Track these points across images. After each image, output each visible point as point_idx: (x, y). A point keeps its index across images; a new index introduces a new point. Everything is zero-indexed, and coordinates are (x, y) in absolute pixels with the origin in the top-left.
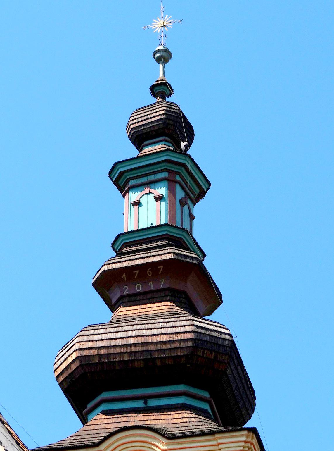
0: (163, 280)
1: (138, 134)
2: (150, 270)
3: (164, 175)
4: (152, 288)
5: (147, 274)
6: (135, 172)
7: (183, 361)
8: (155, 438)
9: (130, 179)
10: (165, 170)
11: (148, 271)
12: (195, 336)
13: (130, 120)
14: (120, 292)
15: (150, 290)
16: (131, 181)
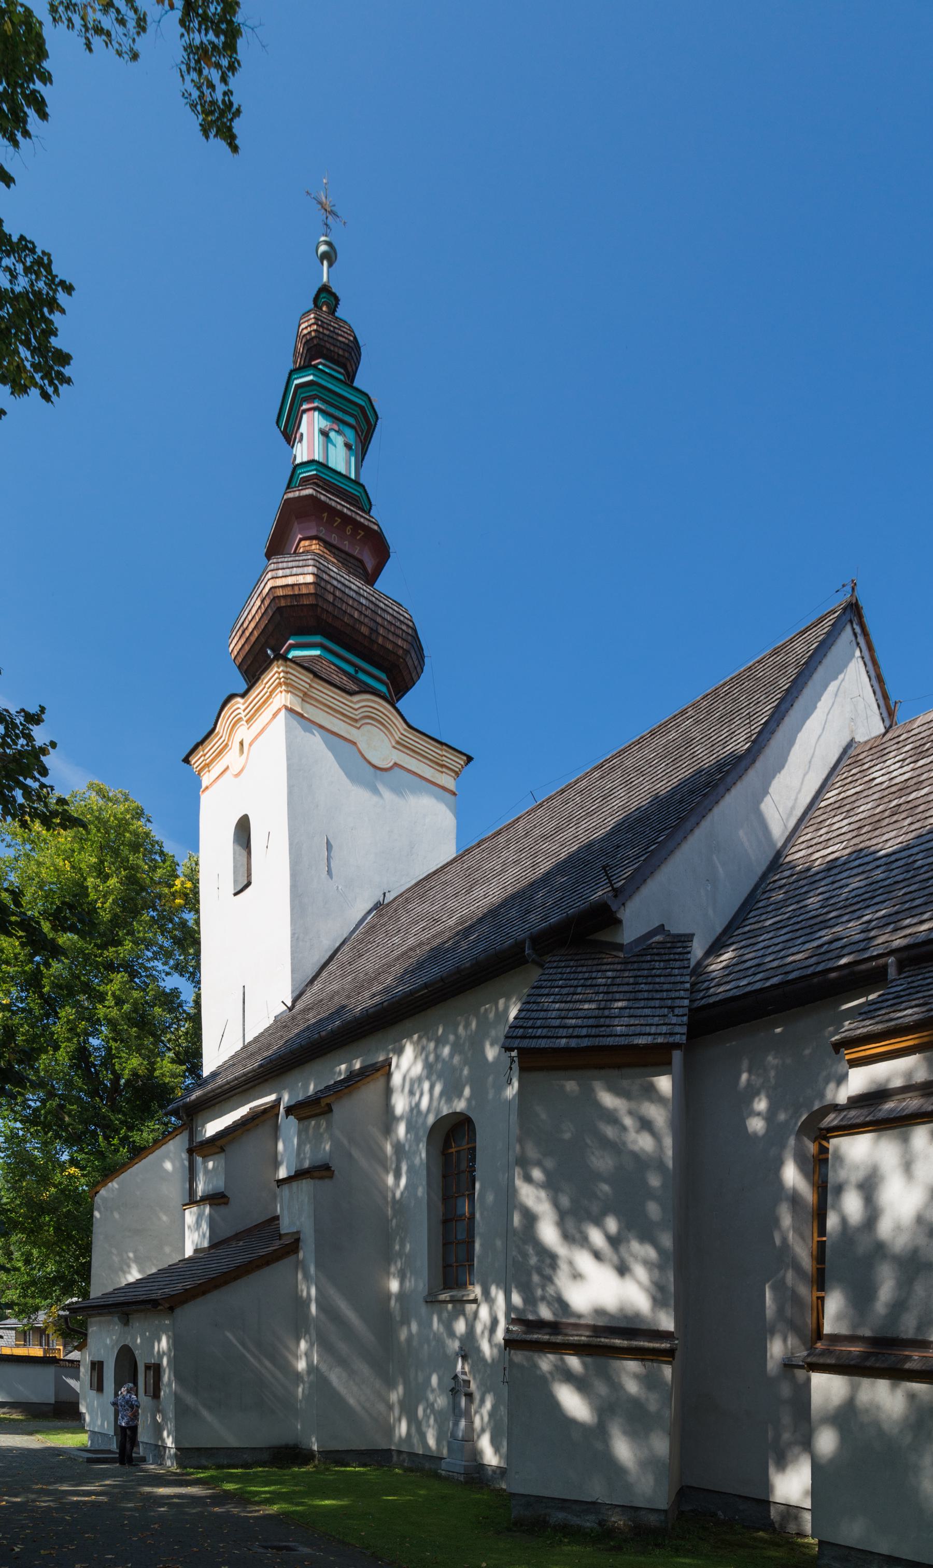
3: (351, 421)
11: (348, 528)
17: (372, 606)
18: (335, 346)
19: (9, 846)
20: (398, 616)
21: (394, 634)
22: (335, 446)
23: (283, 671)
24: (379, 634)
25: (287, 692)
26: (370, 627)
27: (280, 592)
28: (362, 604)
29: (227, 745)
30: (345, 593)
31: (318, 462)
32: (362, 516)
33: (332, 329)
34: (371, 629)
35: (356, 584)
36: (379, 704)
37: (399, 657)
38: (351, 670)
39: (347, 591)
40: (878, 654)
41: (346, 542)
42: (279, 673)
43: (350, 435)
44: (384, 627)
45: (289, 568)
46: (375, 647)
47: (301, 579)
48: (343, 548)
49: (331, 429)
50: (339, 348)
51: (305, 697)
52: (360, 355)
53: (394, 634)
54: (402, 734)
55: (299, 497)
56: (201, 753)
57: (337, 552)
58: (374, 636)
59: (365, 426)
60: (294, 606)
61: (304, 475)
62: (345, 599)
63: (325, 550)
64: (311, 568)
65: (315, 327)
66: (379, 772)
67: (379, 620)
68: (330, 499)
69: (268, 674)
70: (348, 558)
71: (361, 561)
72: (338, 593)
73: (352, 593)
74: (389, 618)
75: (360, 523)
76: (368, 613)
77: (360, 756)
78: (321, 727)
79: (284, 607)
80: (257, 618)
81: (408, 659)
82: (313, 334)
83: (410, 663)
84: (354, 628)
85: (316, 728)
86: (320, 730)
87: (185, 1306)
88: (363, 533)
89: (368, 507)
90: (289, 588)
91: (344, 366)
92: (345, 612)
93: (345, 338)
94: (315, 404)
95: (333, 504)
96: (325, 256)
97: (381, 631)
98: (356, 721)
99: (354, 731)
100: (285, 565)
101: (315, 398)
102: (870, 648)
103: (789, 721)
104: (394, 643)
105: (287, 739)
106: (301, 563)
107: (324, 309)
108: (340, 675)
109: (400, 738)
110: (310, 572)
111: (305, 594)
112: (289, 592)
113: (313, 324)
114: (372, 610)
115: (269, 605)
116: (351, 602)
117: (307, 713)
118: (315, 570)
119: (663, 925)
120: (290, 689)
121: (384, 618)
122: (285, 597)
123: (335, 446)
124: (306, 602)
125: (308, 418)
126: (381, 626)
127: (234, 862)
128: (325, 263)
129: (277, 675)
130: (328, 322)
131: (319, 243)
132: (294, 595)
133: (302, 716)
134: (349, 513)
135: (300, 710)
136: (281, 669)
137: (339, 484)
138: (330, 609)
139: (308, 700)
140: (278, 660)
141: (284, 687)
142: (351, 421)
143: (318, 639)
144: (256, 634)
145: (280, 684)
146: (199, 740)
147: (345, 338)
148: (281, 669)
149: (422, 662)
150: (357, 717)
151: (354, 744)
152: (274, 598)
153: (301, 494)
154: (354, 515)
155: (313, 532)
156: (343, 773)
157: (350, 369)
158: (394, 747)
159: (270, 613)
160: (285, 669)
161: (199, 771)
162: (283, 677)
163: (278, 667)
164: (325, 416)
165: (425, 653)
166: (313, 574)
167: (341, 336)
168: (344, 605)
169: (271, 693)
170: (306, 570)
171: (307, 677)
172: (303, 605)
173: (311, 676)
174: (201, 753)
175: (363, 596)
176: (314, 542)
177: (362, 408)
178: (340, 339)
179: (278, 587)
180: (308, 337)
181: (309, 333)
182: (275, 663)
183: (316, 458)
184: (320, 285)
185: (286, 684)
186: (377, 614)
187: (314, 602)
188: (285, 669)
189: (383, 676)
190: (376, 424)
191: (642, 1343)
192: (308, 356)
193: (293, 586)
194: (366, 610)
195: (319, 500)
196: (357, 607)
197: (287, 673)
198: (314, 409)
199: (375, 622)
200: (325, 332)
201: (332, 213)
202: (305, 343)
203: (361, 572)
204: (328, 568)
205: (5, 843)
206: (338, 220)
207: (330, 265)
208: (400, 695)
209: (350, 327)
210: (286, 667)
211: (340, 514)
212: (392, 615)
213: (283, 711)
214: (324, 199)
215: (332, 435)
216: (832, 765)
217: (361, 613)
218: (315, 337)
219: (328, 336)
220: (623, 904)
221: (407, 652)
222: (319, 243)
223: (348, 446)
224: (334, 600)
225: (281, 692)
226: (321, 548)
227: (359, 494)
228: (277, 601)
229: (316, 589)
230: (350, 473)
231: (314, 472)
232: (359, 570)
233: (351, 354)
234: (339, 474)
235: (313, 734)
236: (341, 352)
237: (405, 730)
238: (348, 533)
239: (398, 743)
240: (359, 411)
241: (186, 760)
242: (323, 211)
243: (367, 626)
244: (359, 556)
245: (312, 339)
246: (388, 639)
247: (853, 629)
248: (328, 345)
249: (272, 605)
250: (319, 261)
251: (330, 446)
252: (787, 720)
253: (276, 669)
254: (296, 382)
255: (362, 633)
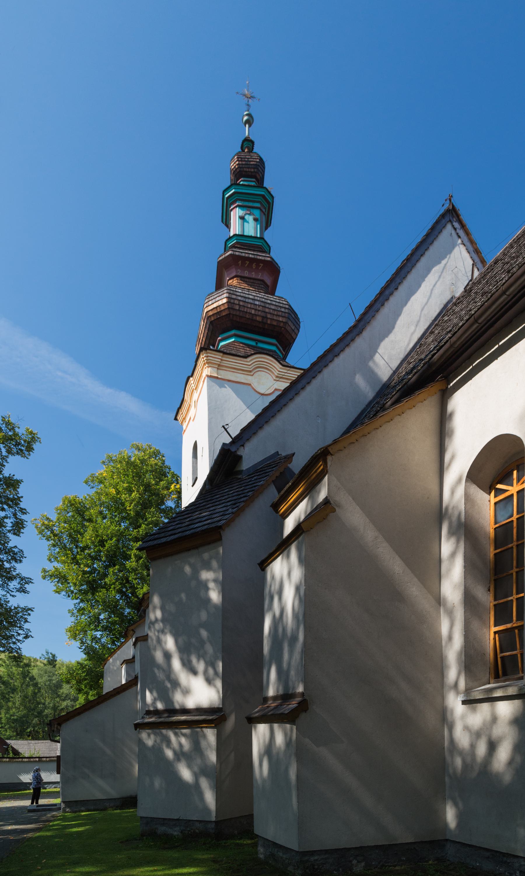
3: (258, 205)
11: (254, 265)
19: (93, 487)
21: (277, 315)
23: (205, 356)
24: (268, 318)
25: (208, 367)
27: (211, 313)
28: (256, 305)
29: (190, 405)
31: (238, 235)
32: (260, 256)
33: (247, 160)
34: (263, 317)
35: (261, 295)
37: (281, 327)
39: (247, 300)
40: (475, 236)
41: (253, 273)
42: (204, 358)
43: (257, 213)
44: (270, 313)
46: (266, 327)
47: (220, 303)
48: (251, 276)
49: (245, 214)
50: (252, 168)
51: (219, 367)
52: (264, 168)
53: (277, 315)
54: (279, 371)
55: (225, 258)
56: (181, 413)
57: (247, 280)
58: (265, 321)
61: (231, 244)
62: (246, 305)
63: (241, 282)
64: (225, 294)
65: (237, 163)
66: (265, 397)
67: (267, 310)
68: (242, 252)
70: (255, 281)
71: (262, 281)
72: (241, 303)
74: (273, 307)
76: (261, 308)
78: (229, 381)
82: (237, 167)
83: (289, 329)
86: (230, 383)
87: (68, 722)
89: (268, 249)
90: (215, 309)
91: (254, 177)
92: (246, 312)
93: (254, 161)
94: (237, 204)
95: (243, 255)
96: (247, 122)
97: (269, 316)
98: (250, 371)
99: (250, 378)
100: (212, 298)
102: (467, 233)
103: (393, 300)
105: (208, 393)
106: (220, 294)
107: (246, 151)
109: (278, 374)
110: (225, 297)
113: (236, 161)
114: (262, 306)
115: (206, 322)
116: (249, 306)
117: (221, 375)
119: (278, 452)
120: (210, 365)
121: (270, 309)
122: (213, 315)
124: (224, 314)
125: (233, 213)
126: (269, 313)
128: (247, 126)
129: (203, 359)
130: (245, 157)
131: (244, 115)
132: (218, 312)
133: (217, 378)
134: (253, 256)
135: (216, 375)
136: (204, 355)
137: (232, 243)
138: (238, 313)
140: (202, 351)
141: (207, 365)
142: (258, 205)
143: (233, 332)
144: (204, 340)
145: (205, 364)
146: (178, 406)
147: (254, 161)
148: (204, 355)
149: (297, 326)
150: (251, 369)
151: (250, 385)
154: (256, 257)
155: (234, 274)
157: (259, 177)
158: (275, 380)
159: (208, 326)
162: (206, 360)
164: (242, 208)
165: (301, 320)
166: (226, 297)
167: (252, 161)
168: (246, 308)
169: (202, 370)
171: (220, 356)
172: (223, 316)
173: (221, 354)
174: (181, 413)
175: (257, 300)
176: (235, 279)
177: (263, 196)
179: (209, 311)
180: (234, 169)
181: (235, 167)
182: (201, 353)
183: (237, 233)
184: (243, 139)
186: (265, 307)
187: (228, 313)
189: (274, 341)
190: (273, 201)
191: (179, 718)
192: (236, 179)
193: (216, 307)
194: (259, 307)
195: (236, 255)
196: (254, 307)
197: (207, 357)
198: (236, 207)
199: (265, 312)
201: (252, 97)
202: (233, 173)
203: (263, 286)
204: (236, 291)
205: (90, 487)
206: (255, 100)
207: (250, 126)
208: (287, 348)
209: (258, 154)
210: (207, 353)
211: (248, 259)
212: (275, 305)
214: (246, 92)
215: (247, 217)
216: (433, 319)
217: (256, 310)
218: (238, 168)
219: (245, 164)
220: (243, 446)
221: (286, 323)
222: (244, 115)
223: (256, 220)
224: (239, 307)
225: (206, 368)
226: (238, 281)
227: (261, 244)
229: (228, 305)
230: (257, 234)
231: (235, 241)
232: (261, 286)
233: (258, 169)
234: (251, 237)
235: (225, 387)
236: (252, 170)
237: (281, 368)
238: (254, 268)
239: (277, 377)
240: (262, 198)
241: (176, 419)
242: (246, 98)
244: (262, 278)
245: (236, 170)
246: (274, 319)
247: (453, 226)
248: (245, 169)
249: (208, 322)
250: (244, 125)
251: (245, 224)
252: (392, 299)
254: (227, 196)
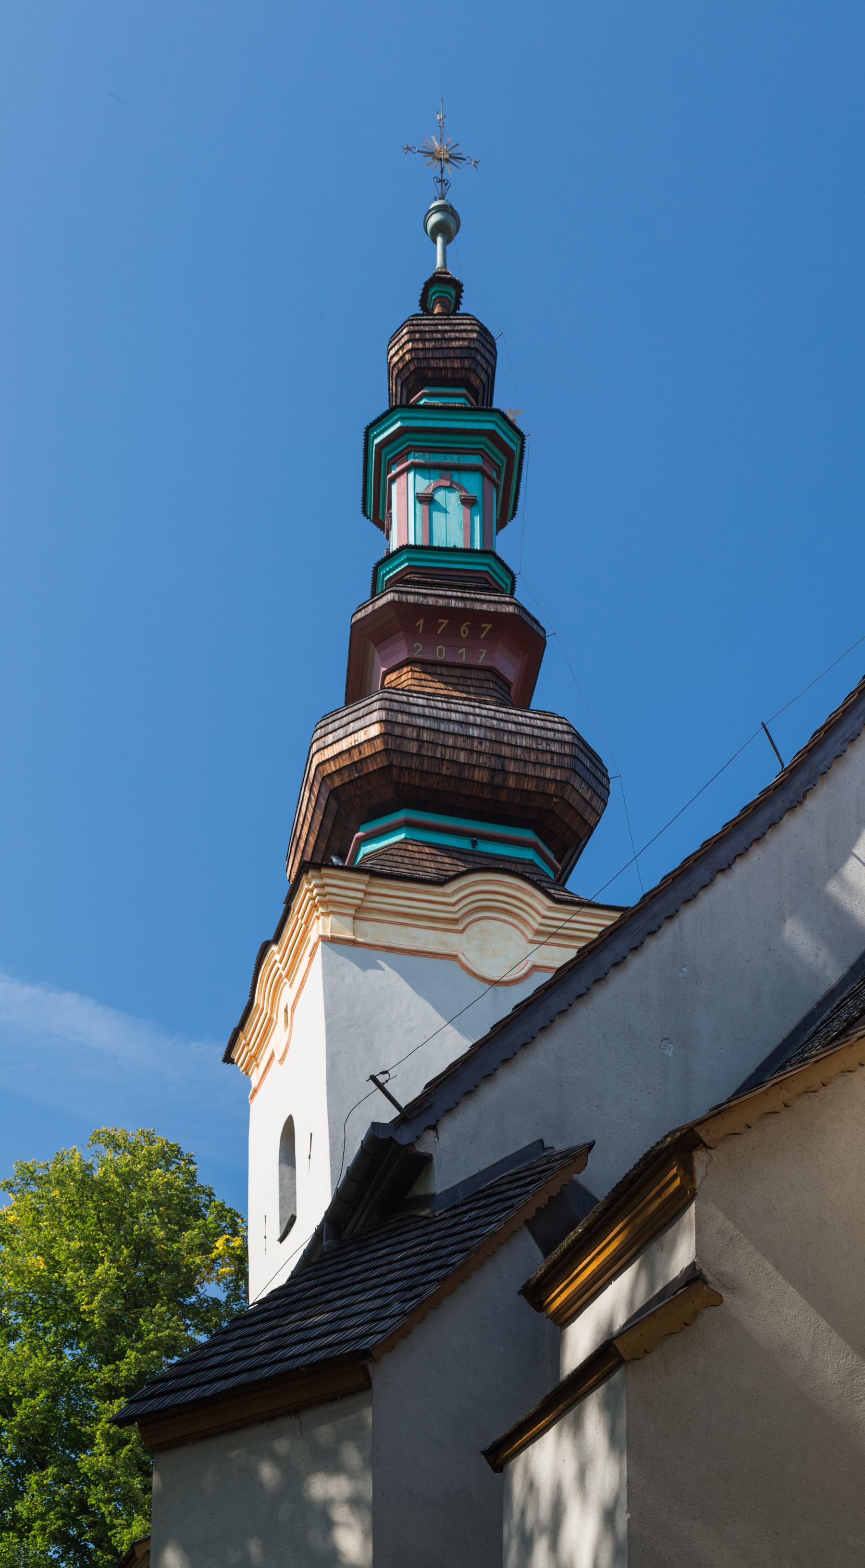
0: (485, 651)
1: (419, 365)
2: (467, 626)
3: (475, 460)
4: (464, 660)
5: (460, 633)
6: (392, 445)
7: (551, 791)
8: (532, 895)
9: (413, 449)
10: (480, 452)
11: (463, 627)
12: (466, 759)
13: (406, 324)
14: (408, 651)
15: (458, 661)
16: (413, 453)
17: (492, 735)
18: (444, 359)
20: (544, 733)
22: (446, 512)
26: (489, 768)
27: (332, 767)
28: (472, 737)
29: (271, 1019)
30: (439, 731)
36: (498, 883)
38: (464, 844)
39: (443, 727)
42: (312, 891)
43: (473, 483)
44: (516, 759)
45: (342, 727)
46: (504, 796)
47: (361, 737)
51: (359, 912)
54: (544, 917)
55: (373, 612)
56: (244, 1042)
57: (444, 671)
58: (498, 780)
59: (501, 459)
60: (356, 779)
62: (440, 739)
65: (410, 345)
67: (506, 751)
68: (425, 595)
69: (299, 897)
70: (467, 673)
72: (425, 736)
73: (452, 728)
75: (482, 612)
76: (485, 747)
77: (464, 973)
78: (390, 949)
79: (340, 786)
80: (309, 816)
81: (568, 794)
82: (407, 357)
83: (573, 799)
84: (460, 779)
85: (382, 953)
88: (489, 626)
89: (508, 581)
91: (465, 383)
93: (463, 339)
95: (431, 601)
96: (439, 228)
97: (511, 767)
98: (456, 921)
99: (454, 938)
101: (409, 453)
104: (537, 777)
108: (439, 859)
109: (541, 924)
110: (374, 720)
111: (369, 756)
112: (345, 761)
117: (365, 935)
118: (382, 715)
119: (542, 1141)
122: (339, 771)
123: (446, 512)
127: (280, 1192)
128: (439, 240)
133: (354, 943)
134: (460, 605)
135: (350, 936)
138: (415, 764)
139: (366, 915)
141: (321, 910)
144: (312, 840)
145: (315, 906)
147: (463, 339)
150: (457, 916)
151: (454, 957)
152: (323, 778)
153: (376, 607)
154: (469, 605)
155: (403, 656)
156: (432, 1009)
158: (532, 942)
159: (323, 802)
160: (319, 882)
161: (245, 1069)
162: (318, 895)
163: (309, 883)
170: (367, 720)
173: (366, 878)
174: (244, 1042)
176: (405, 670)
177: (491, 435)
178: (455, 344)
179: (328, 760)
180: (400, 365)
181: (402, 358)
185: (323, 903)
187: (386, 763)
188: (319, 882)
193: (349, 750)
194: (481, 743)
198: (407, 470)
200: (428, 345)
202: (397, 375)
207: (447, 241)
210: (321, 877)
211: (447, 611)
213: (320, 944)
215: (440, 496)
217: (471, 751)
218: (412, 360)
220: (434, 1128)
223: (468, 502)
225: (318, 918)
226: (416, 675)
227: (486, 568)
228: (328, 782)
231: (407, 564)
234: (454, 550)
236: (457, 364)
237: (550, 909)
239: (538, 932)
241: (228, 1059)
243: (484, 768)
245: (406, 365)
248: (433, 363)
249: (323, 790)
253: (306, 886)
254: (377, 441)
255: (477, 782)
